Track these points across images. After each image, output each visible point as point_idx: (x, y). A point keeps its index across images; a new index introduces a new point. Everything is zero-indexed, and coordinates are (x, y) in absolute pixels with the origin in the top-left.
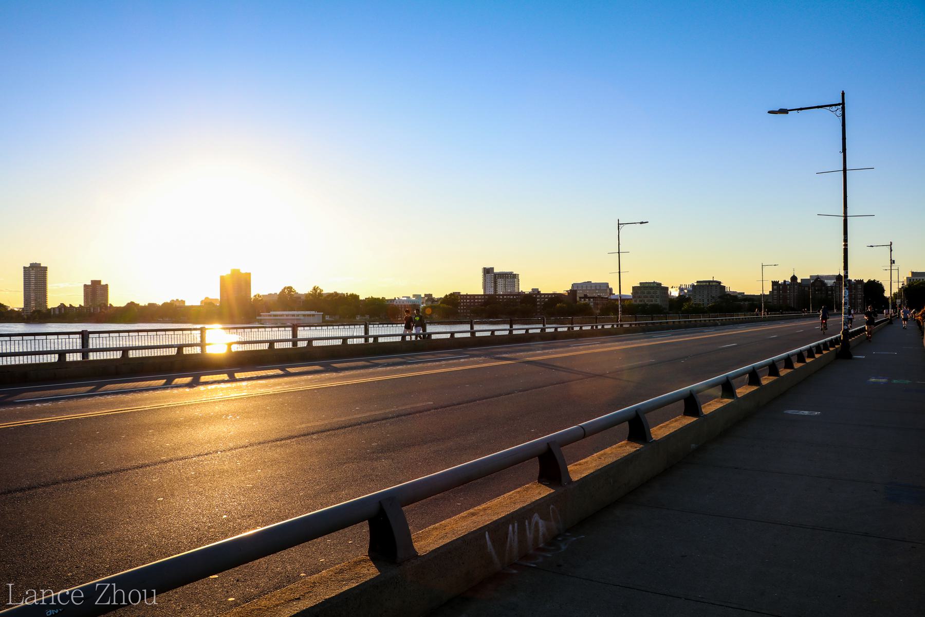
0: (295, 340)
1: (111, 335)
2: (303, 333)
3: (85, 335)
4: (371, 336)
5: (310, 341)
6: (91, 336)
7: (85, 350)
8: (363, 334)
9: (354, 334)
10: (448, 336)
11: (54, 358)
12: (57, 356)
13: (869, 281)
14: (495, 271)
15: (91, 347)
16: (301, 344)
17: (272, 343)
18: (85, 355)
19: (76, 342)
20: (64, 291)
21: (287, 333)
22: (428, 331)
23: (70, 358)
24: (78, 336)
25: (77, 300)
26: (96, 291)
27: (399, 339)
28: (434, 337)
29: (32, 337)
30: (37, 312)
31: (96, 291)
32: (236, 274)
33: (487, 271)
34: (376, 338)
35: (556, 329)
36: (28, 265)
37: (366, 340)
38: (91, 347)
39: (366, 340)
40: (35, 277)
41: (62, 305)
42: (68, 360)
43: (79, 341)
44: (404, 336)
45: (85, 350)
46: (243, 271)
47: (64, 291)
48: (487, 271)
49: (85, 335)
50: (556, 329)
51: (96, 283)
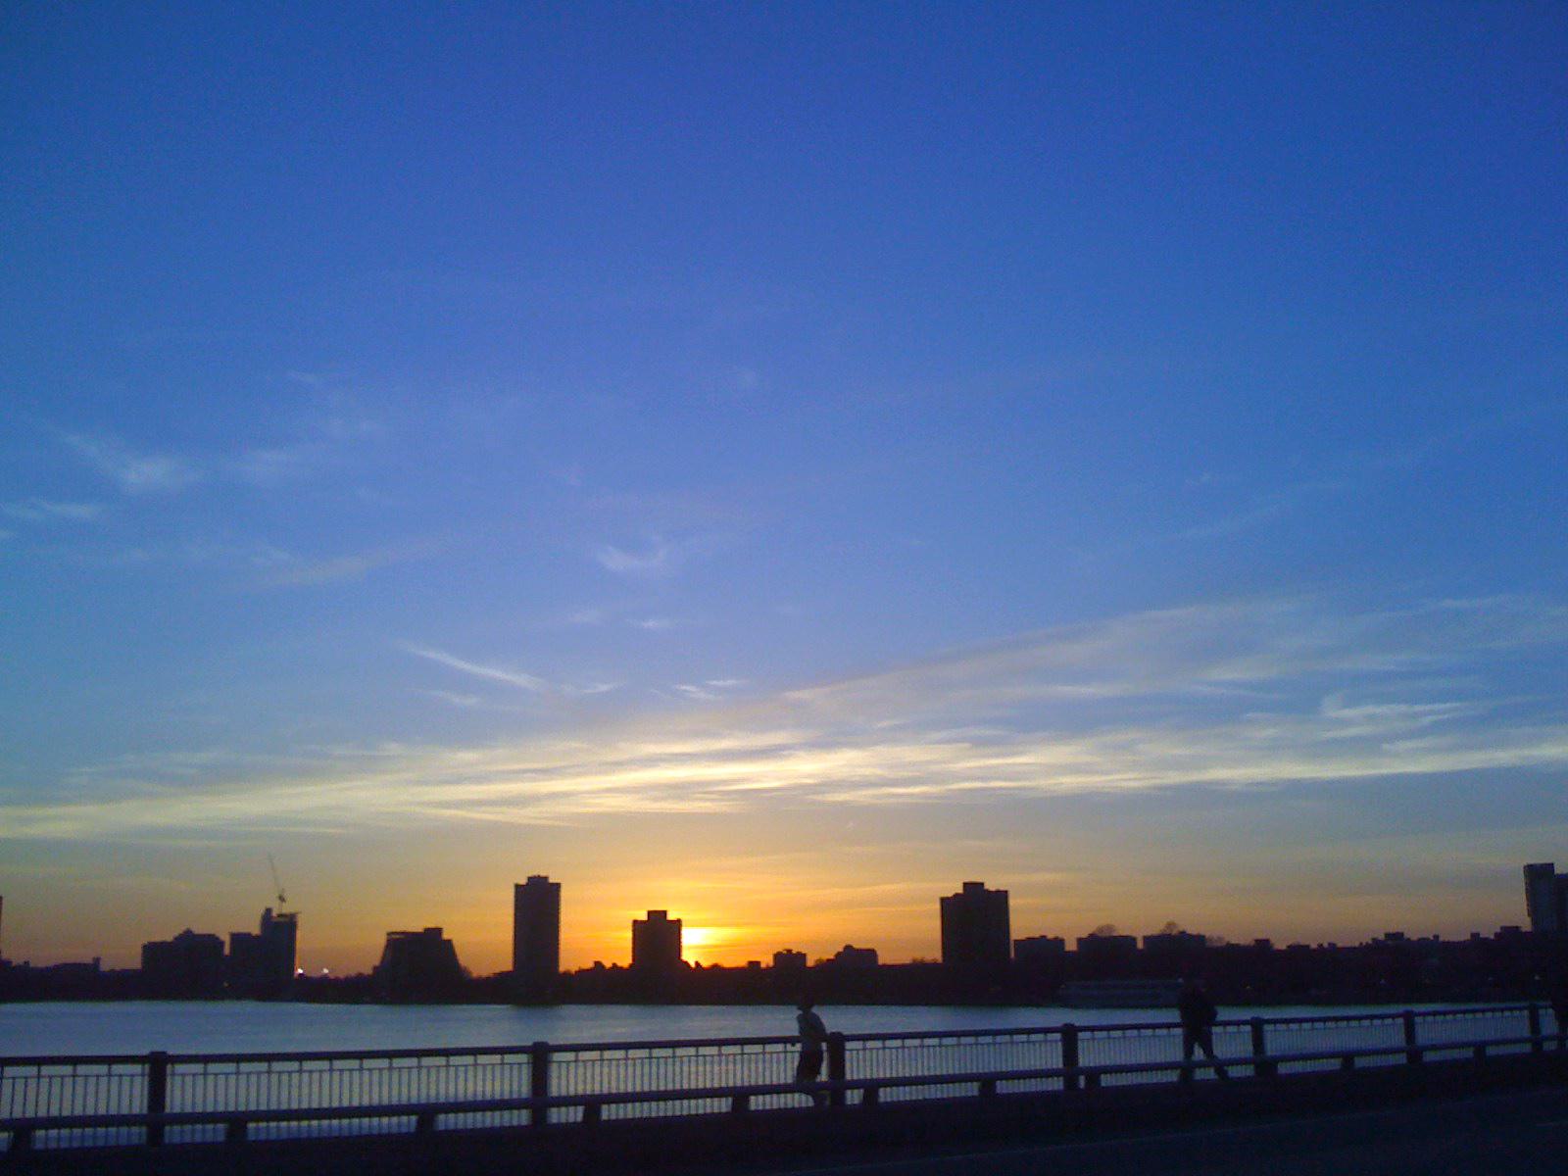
1: (117, 1069)
3: (1070, 1034)
4: (855, 1084)
5: (592, 1103)
8: (1526, 1033)
9: (900, 1063)
12: (581, 1109)
13: (449, 942)
15: (848, 1077)
17: (740, 1095)
20: (596, 932)
22: (1085, 1060)
23: (1234, 1072)
25: (619, 950)
26: (657, 934)
27: (1173, 1076)
28: (1283, 1068)
29: (68, 1069)
30: (537, 972)
31: (657, 934)
32: (973, 889)
34: (871, 1087)
36: (523, 881)
40: (538, 904)
44: (1187, 1068)
47: (596, 932)
49: (1070, 1034)
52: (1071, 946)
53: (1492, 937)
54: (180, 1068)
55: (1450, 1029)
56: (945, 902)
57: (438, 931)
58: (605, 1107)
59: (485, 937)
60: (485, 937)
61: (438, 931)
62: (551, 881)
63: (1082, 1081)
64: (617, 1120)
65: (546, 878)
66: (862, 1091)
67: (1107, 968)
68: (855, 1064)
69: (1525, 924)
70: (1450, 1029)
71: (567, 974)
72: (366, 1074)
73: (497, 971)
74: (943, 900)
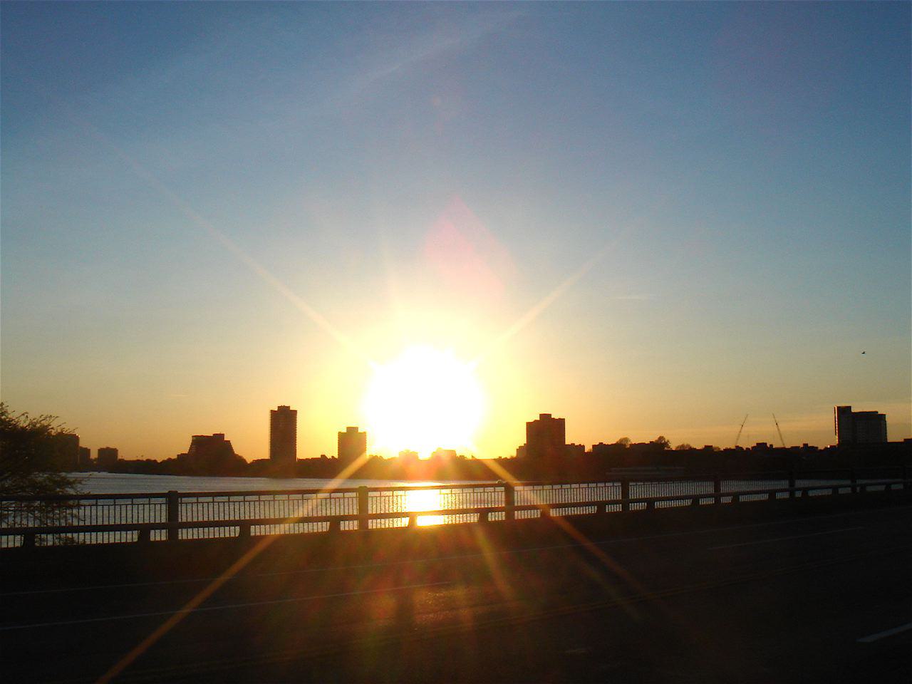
0: (717, 495)
2: (637, 491)
3: (173, 500)
4: (799, 489)
6: (370, 494)
7: (173, 524)
10: (765, 497)
11: (132, 537)
12: (238, 528)
14: (853, 410)
15: (370, 512)
16: (726, 500)
18: (172, 534)
19: (159, 513)
21: (708, 488)
24: (163, 500)
32: (545, 418)
33: (843, 412)
35: (888, 485)
37: (792, 494)
38: (370, 512)
39: (792, 494)
40: (284, 421)
41: (323, 456)
42: (152, 539)
43: (503, 496)
45: (173, 524)
46: (555, 416)
47: (316, 440)
48: (843, 412)
50: (888, 485)
51: (352, 431)
52: (588, 448)
53: (745, 449)
54: (184, 500)
55: (819, 488)
56: (529, 424)
57: (222, 436)
58: (152, 532)
59: (253, 443)
60: (253, 443)
61: (222, 436)
62: (879, 413)
63: (858, 489)
64: (126, 543)
65: (877, 412)
66: (328, 523)
67: (616, 461)
68: (548, 498)
69: (336, 456)
70: (819, 488)
71: (896, 445)
72: (152, 506)
73: (255, 459)
74: (528, 423)
